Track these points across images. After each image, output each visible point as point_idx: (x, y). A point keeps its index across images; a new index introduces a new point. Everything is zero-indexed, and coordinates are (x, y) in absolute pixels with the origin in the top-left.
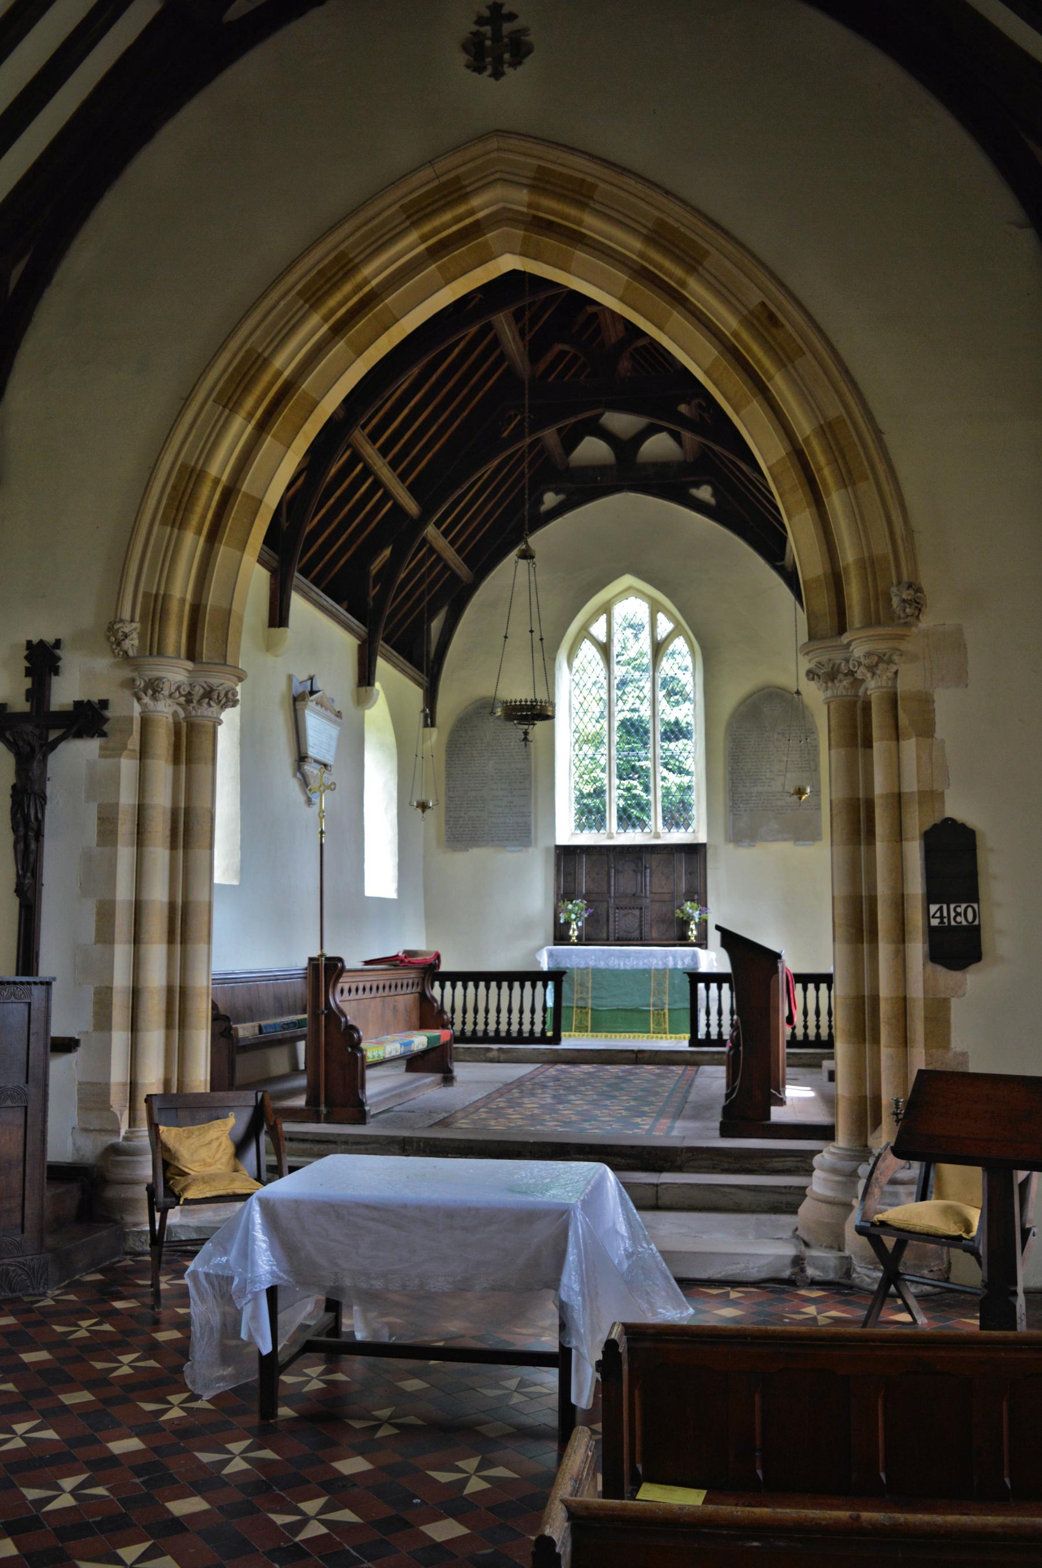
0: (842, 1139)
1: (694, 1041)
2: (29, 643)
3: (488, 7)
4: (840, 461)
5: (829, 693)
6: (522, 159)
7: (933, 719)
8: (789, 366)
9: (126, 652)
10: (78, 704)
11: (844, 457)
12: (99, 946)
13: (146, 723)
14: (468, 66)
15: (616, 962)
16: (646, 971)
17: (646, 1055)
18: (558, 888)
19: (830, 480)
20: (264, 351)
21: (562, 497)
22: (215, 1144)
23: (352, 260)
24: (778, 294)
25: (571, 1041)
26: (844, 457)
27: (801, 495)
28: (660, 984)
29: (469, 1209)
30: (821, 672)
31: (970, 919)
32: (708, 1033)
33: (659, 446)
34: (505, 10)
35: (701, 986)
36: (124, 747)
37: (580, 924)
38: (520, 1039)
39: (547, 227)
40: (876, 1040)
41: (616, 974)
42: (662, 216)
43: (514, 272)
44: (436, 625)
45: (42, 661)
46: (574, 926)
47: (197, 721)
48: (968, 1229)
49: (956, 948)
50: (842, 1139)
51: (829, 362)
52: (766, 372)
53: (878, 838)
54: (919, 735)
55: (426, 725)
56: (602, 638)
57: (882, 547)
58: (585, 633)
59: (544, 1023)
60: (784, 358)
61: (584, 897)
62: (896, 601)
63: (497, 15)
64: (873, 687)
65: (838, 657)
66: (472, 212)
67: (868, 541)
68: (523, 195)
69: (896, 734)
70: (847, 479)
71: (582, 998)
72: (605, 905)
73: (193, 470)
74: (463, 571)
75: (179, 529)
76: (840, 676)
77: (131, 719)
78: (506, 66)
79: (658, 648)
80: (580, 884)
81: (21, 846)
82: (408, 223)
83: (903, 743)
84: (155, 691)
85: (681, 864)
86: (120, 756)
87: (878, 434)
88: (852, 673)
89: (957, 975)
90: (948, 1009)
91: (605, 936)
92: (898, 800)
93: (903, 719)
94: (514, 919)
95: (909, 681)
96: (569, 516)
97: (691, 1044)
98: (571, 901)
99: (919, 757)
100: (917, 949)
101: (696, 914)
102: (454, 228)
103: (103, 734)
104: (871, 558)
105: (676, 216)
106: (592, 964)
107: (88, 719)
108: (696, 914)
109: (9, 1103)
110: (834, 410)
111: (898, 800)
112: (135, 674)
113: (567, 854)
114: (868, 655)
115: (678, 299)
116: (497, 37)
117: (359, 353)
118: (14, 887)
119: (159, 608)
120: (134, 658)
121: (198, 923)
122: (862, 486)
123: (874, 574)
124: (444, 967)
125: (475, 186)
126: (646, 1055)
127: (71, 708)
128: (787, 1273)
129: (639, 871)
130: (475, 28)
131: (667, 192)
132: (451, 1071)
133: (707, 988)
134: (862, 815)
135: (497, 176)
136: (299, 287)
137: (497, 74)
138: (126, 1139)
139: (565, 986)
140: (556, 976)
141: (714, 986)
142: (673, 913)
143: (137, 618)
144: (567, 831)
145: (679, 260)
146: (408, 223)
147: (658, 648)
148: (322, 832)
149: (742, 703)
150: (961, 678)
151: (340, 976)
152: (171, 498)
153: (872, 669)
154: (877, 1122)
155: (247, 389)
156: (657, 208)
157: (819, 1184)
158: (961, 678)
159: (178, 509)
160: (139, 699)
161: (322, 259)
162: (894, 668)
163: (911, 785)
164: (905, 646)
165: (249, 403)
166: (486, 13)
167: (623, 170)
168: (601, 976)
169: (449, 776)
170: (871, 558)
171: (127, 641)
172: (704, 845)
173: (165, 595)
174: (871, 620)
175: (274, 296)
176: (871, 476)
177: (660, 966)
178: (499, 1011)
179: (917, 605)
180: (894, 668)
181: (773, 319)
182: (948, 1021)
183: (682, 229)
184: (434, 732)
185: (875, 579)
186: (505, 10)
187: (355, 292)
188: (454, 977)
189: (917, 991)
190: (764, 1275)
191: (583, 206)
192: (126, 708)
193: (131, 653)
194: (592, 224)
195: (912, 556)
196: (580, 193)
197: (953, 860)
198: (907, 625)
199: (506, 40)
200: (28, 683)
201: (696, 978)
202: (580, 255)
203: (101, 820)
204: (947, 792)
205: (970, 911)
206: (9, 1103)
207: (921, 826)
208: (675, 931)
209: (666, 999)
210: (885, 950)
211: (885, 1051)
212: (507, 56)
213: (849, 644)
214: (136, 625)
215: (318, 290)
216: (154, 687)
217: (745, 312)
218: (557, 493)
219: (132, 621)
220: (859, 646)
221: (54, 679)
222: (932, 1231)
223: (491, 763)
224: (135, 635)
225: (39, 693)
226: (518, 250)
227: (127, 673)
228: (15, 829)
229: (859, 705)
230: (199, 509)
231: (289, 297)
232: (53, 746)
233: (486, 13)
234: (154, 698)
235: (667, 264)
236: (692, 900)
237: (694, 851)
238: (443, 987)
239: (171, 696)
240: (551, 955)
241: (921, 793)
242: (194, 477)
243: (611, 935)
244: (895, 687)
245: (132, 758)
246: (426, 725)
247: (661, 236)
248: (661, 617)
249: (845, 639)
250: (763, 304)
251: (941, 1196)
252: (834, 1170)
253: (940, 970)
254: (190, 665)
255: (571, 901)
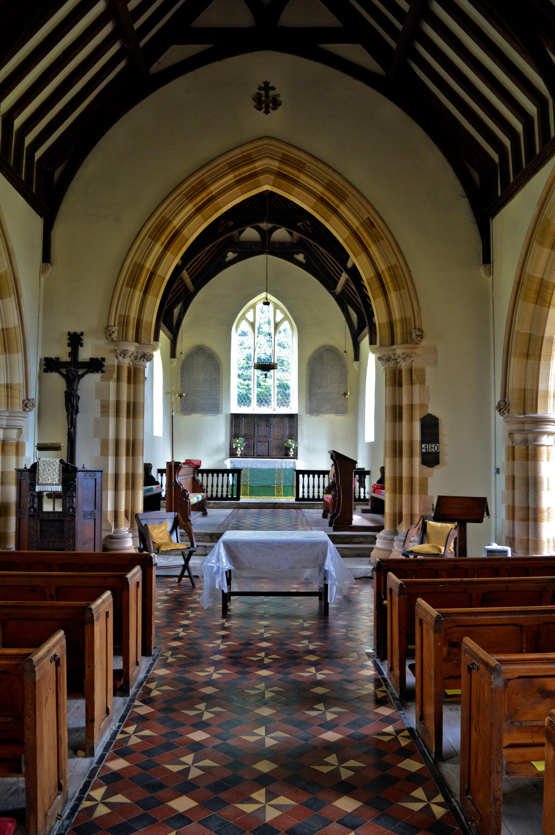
0: (387, 528)
1: (298, 499)
2: (69, 333)
3: (264, 83)
4: (395, 281)
5: (386, 366)
6: (276, 149)
7: (425, 378)
8: (378, 243)
9: (112, 339)
10: (92, 359)
11: (396, 280)
12: (102, 457)
13: (119, 368)
14: (255, 107)
15: (260, 465)
16: (273, 469)
17: (278, 505)
18: (231, 432)
19: (391, 288)
20: (169, 217)
21: (236, 255)
22: (164, 532)
23: (206, 183)
24: (375, 216)
25: (244, 499)
26: (396, 280)
27: (379, 291)
28: (279, 475)
29: (295, 542)
30: (384, 358)
31: (436, 449)
32: (303, 496)
33: (281, 234)
34: (270, 85)
35: (301, 476)
36: (112, 377)
37: (242, 449)
38: (222, 498)
39: (284, 176)
40: (401, 492)
41: (260, 470)
42: (331, 179)
43: (267, 190)
44: (176, 311)
45: (75, 340)
46: (239, 449)
47: (138, 367)
48: (440, 551)
49: (431, 460)
50: (387, 528)
51: (393, 243)
52: (368, 244)
53: (404, 420)
54: (420, 384)
55: (171, 357)
56: (252, 320)
57: (409, 314)
58: (243, 317)
59: (227, 492)
60: (376, 239)
61: (244, 437)
62: (413, 334)
63: (267, 87)
64: (404, 365)
65: (391, 353)
66: (255, 168)
67: (404, 310)
68: (277, 164)
69: (411, 383)
70: (398, 287)
71: (245, 481)
72: (253, 440)
73: (139, 265)
74: (191, 287)
75: (134, 289)
76: (391, 360)
77: (115, 366)
78: (270, 109)
79: (277, 325)
80: (242, 431)
81: (70, 417)
82: (230, 170)
83: (413, 386)
84: (124, 355)
85: (287, 420)
86: (110, 381)
87: (409, 272)
88: (396, 359)
89: (430, 469)
90: (427, 481)
91: (252, 454)
92: (411, 407)
93: (414, 378)
94: (211, 447)
95: (417, 364)
96: (239, 264)
97: (296, 501)
98: (238, 439)
99: (420, 391)
100: (417, 460)
101: (293, 445)
102: (247, 174)
103: (103, 372)
104: (405, 318)
105: (337, 180)
106: (249, 466)
107: (96, 365)
108: (293, 445)
109: (89, 517)
110: (394, 262)
111: (411, 407)
112: (116, 348)
113: (236, 418)
114: (403, 354)
115: (335, 211)
116: (267, 96)
117: (206, 221)
118: (67, 433)
119: (125, 321)
120: (115, 341)
121: (138, 448)
122: (403, 291)
123: (406, 324)
124: (203, 467)
125: (257, 158)
126: (278, 505)
127: (88, 361)
128: (370, 575)
129: (268, 425)
130: (258, 91)
131: (335, 171)
132: (206, 511)
133: (303, 477)
134: (397, 411)
135: (267, 155)
136: (184, 193)
137: (267, 112)
138: (114, 533)
139: (242, 476)
140: (237, 472)
141: (306, 476)
142: (283, 444)
143: (116, 325)
144: (236, 408)
145: (338, 198)
146: (230, 170)
147: (277, 325)
148: (172, 411)
149: (315, 352)
150: (435, 363)
151: (180, 469)
152: (130, 276)
153: (404, 359)
154: (401, 521)
155: (162, 233)
156: (331, 176)
157: (379, 544)
158: (435, 363)
159: (133, 281)
160: (117, 358)
161: (195, 181)
162: (412, 359)
163: (416, 401)
164: (416, 351)
165: (163, 239)
166: (263, 85)
167: (318, 160)
168: (254, 471)
169: (182, 381)
170: (405, 318)
171: (114, 334)
172: (297, 415)
173: (128, 316)
174: (405, 342)
175: (174, 195)
176: (406, 288)
177: (280, 468)
178: (212, 486)
179: (422, 337)
180: (412, 359)
181: (372, 224)
182: (427, 485)
183: (339, 185)
184: (175, 361)
185: (406, 326)
186: (270, 85)
187: (207, 196)
188: (207, 472)
189: (417, 475)
190: (362, 576)
191: (300, 171)
192: (111, 361)
193: (114, 339)
194: (303, 178)
195: (420, 319)
196: (300, 166)
197: (431, 428)
198: (417, 343)
199: (271, 98)
200: (69, 349)
201: (299, 472)
202: (296, 189)
203: (102, 406)
204: (429, 405)
205: (436, 447)
206: (89, 517)
207: (420, 415)
208: (283, 452)
209: (282, 481)
210: (405, 460)
211: (404, 496)
212: (271, 105)
213: (395, 349)
214: (116, 328)
215: (192, 194)
216: (124, 353)
217: (362, 221)
218: (234, 253)
219: (115, 326)
220: (399, 350)
221: (80, 348)
222: (428, 553)
223: (202, 375)
224: (116, 332)
225: (74, 354)
226: (271, 183)
227: (112, 347)
228: (67, 410)
229: (397, 371)
230: (141, 281)
231: (180, 196)
232: (82, 376)
233: (263, 85)
234: (124, 357)
235: (332, 198)
236: (292, 439)
237: (292, 417)
238: (202, 476)
239: (130, 357)
240: (231, 462)
241: (420, 405)
242: (140, 268)
243: (255, 453)
244: (412, 366)
245: (114, 381)
246: (171, 357)
247: (330, 187)
248: (278, 311)
249: (394, 347)
250: (369, 218)
251: (428, 542)
252: (386, 539)
253: (425, 467)
254: (137, 344)
255: (238, 439)
